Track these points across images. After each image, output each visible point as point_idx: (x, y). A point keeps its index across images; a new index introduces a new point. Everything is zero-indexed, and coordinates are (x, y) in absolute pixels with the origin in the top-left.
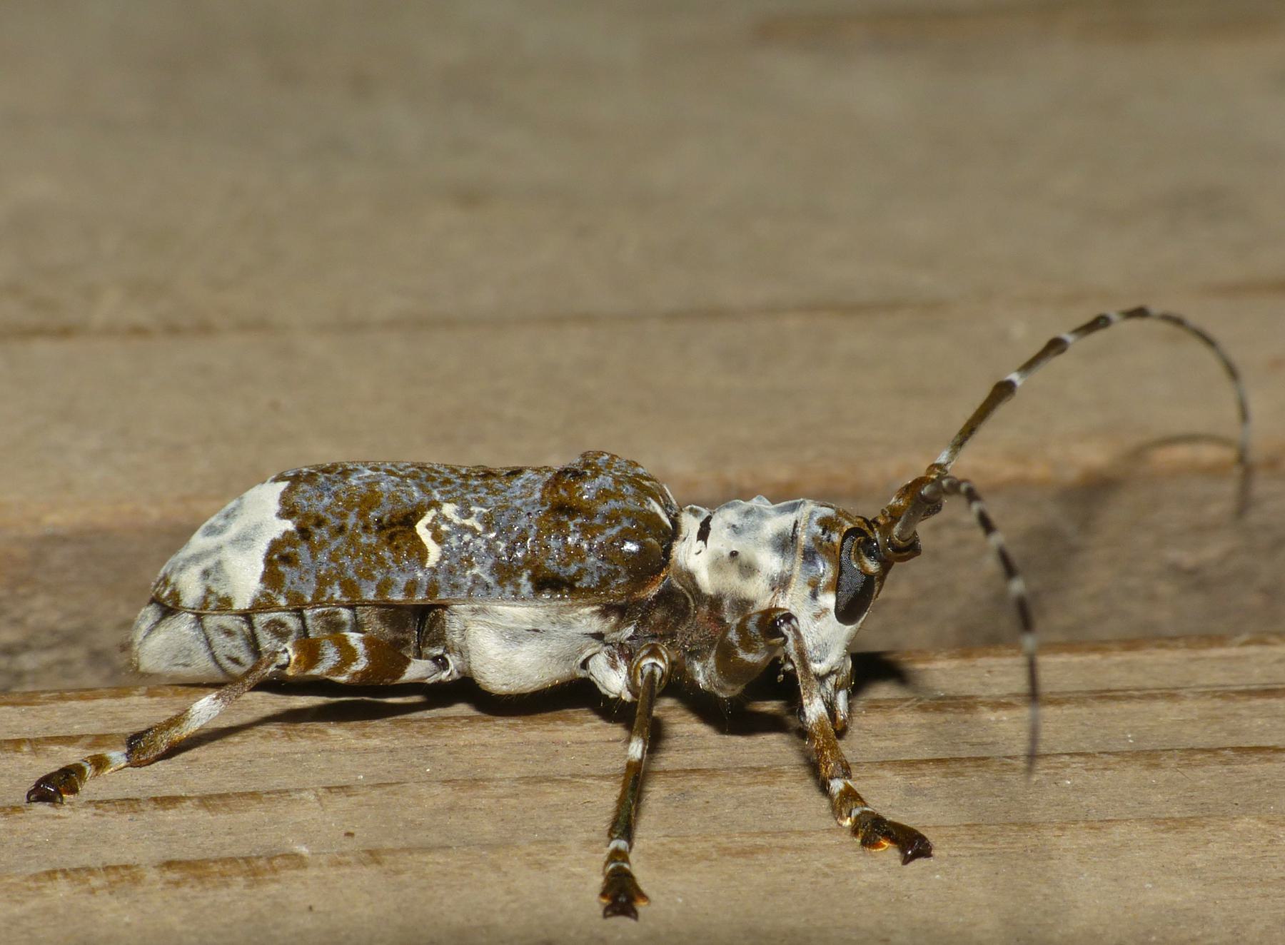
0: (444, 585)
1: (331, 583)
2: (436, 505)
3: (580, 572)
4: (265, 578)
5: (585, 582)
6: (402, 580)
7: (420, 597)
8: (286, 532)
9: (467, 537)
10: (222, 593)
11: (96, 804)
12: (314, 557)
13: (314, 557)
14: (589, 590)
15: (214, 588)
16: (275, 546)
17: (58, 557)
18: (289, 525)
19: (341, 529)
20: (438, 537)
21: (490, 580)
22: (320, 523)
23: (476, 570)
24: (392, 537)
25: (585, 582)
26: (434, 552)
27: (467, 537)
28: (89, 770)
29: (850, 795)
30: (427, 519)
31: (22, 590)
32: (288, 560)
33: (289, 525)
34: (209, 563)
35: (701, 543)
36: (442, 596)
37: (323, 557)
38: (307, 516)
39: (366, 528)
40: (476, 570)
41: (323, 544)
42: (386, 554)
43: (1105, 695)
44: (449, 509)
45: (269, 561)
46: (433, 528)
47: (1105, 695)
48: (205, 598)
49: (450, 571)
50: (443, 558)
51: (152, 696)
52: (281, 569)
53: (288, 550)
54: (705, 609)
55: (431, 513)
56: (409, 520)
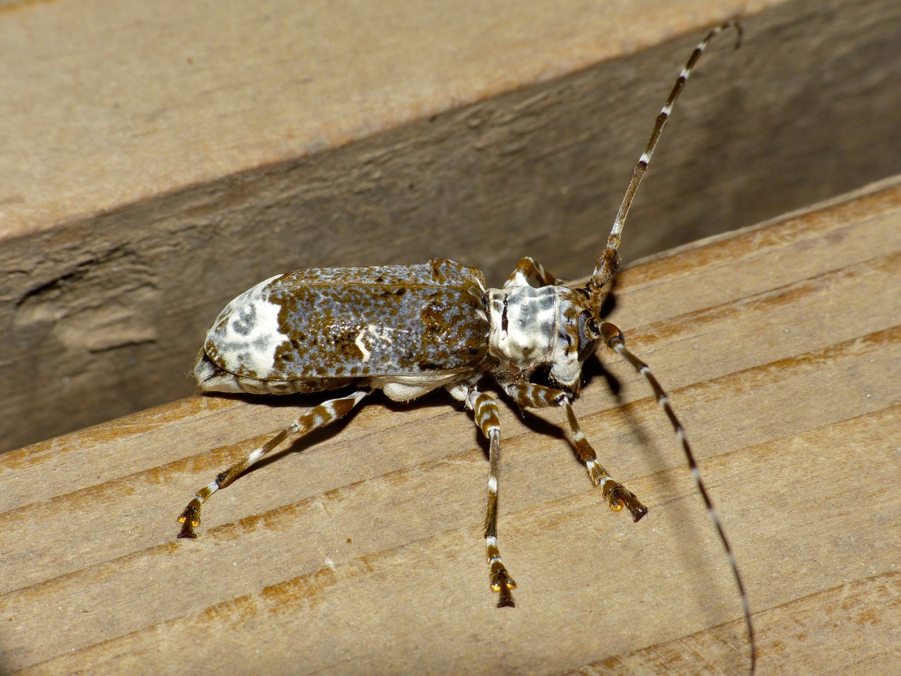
0: (372, 368)
1: (311, 369)
2: (363, 325)
3: (445, 363)
4: (274, 366)
5: (448, 366)
6: (349, 367)
7: (359, 374)
8: (285, 343)
9: (384, 346)
10: (251, 369)
11: (214, 531)
12: (301, 357)
13: (301, 357)
14: (450, 368)
15: (246, 366)
16: (279, 350)
17: (106, 221)
18: (285, 338)
19: (315, 342)
20: (368, 346)
21: (397, 367)
22: (303, 338)
23: (390, 363)
24: (343, 347)
25: (448, 366)
26: (367, 355)
27: (384, 346)
28: (201, 500)
29: (599, 471)
30: (361, 336)
31: (88, 239)
32: (286, 358)
33: (285, 338)
34: (242, 352)
35: (504, 332)
36: (370, 373)
37: (306, 356)
38: (295, 333)
39: (328, 341)
40: (390, 363)
41: (306, 350)
42: (341, 356)
43: (700, 316)
44: (372, 328)
45: (277, 359)
46: (364, 340)
47: (700, 316)
48: (241, 369)
49: (375, 363)
50: (371, 357)
51: (211, 409)
52: (284, 362)
53: (287, 353)
54: (507, 363)
55: (363, 332)
56: (351, 336)
